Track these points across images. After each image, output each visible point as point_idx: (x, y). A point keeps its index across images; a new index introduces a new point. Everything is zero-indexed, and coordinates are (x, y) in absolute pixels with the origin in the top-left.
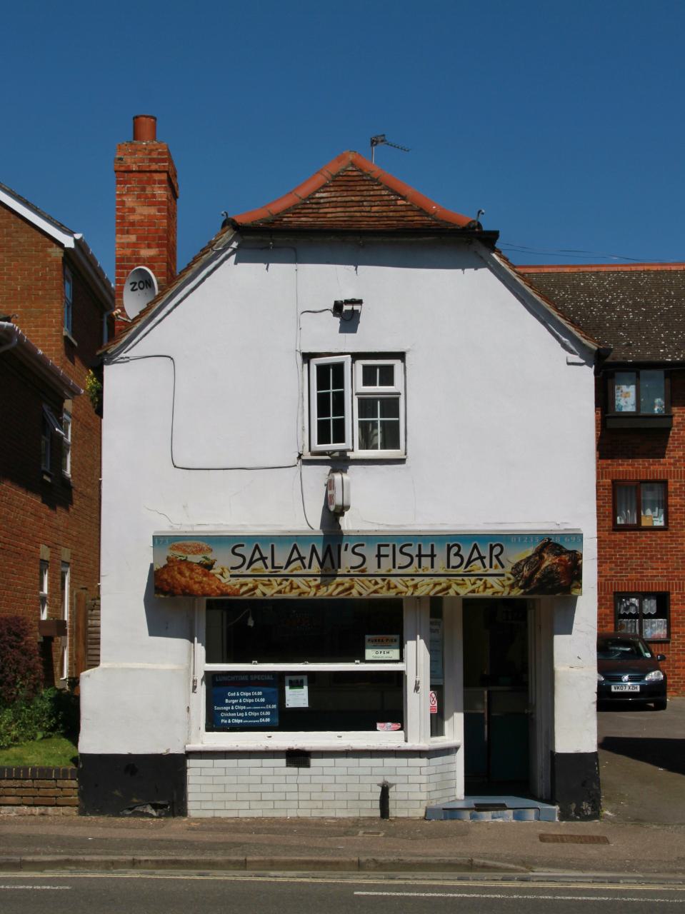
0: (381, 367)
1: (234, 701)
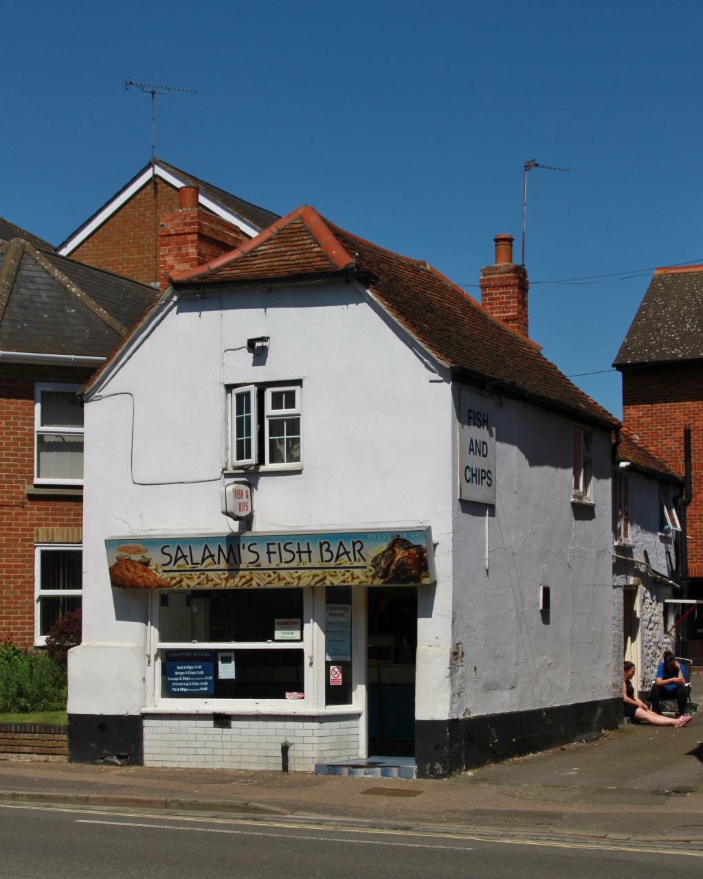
0: (286, 392)
1: (182, 673)
